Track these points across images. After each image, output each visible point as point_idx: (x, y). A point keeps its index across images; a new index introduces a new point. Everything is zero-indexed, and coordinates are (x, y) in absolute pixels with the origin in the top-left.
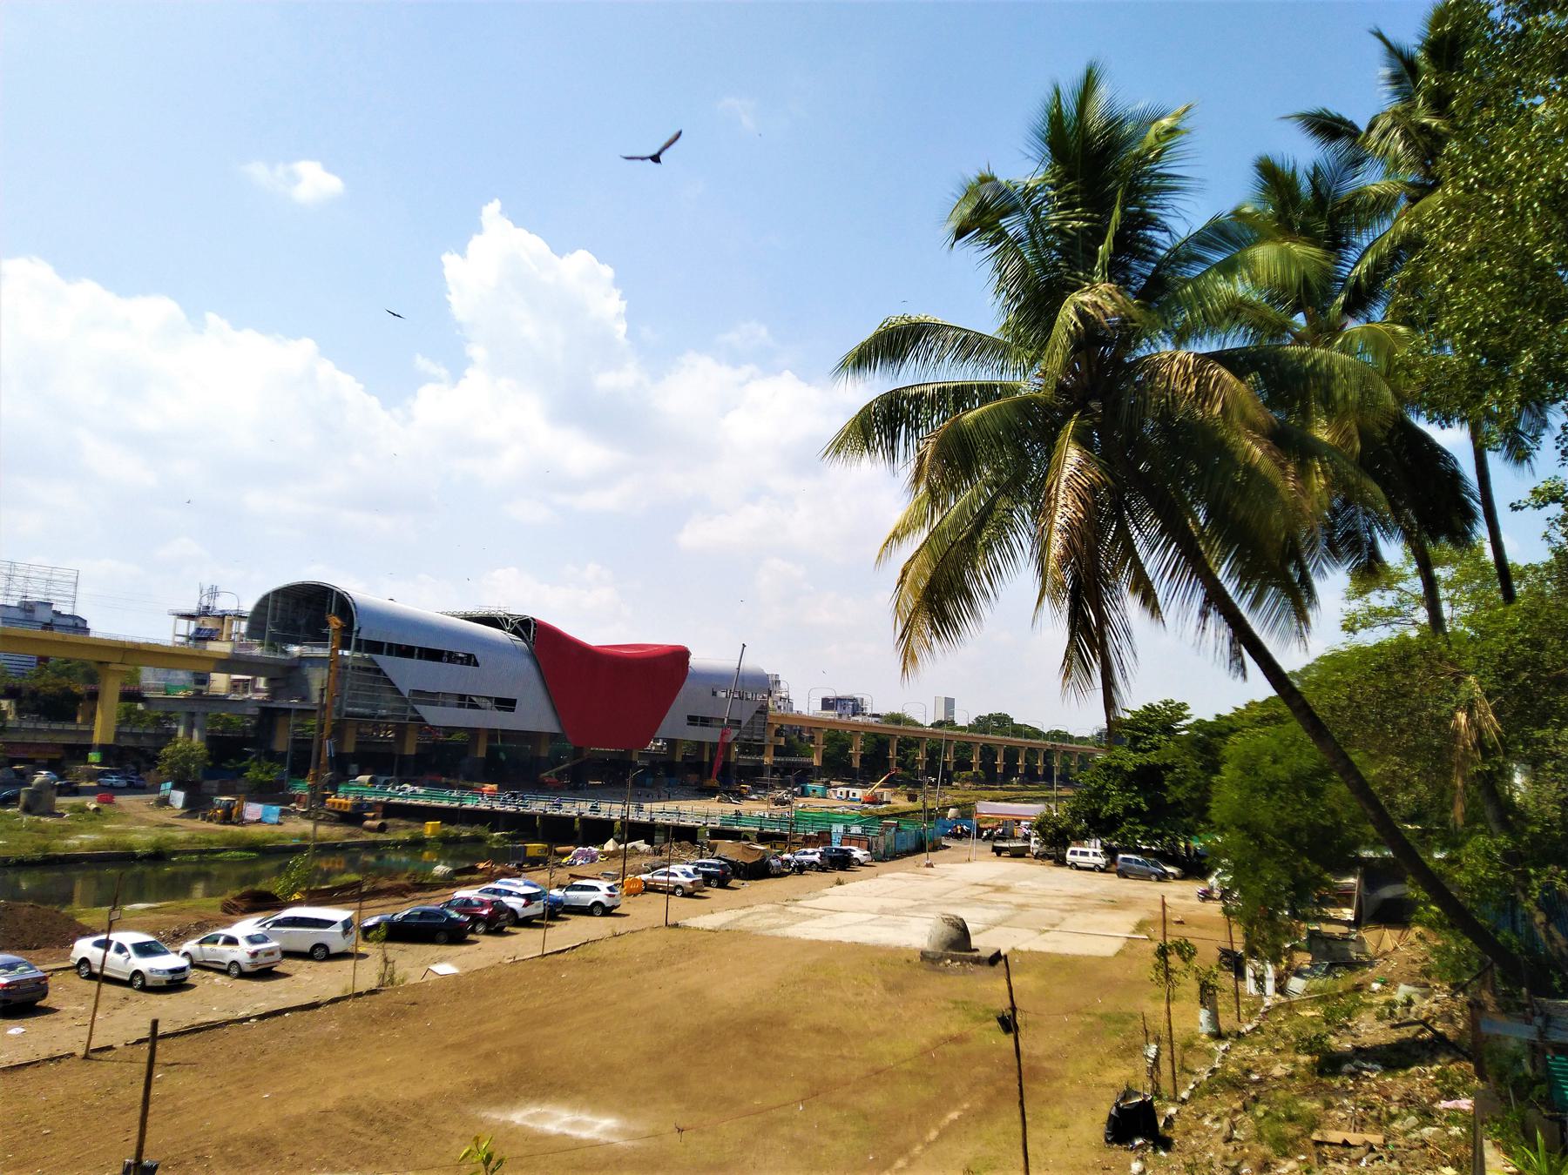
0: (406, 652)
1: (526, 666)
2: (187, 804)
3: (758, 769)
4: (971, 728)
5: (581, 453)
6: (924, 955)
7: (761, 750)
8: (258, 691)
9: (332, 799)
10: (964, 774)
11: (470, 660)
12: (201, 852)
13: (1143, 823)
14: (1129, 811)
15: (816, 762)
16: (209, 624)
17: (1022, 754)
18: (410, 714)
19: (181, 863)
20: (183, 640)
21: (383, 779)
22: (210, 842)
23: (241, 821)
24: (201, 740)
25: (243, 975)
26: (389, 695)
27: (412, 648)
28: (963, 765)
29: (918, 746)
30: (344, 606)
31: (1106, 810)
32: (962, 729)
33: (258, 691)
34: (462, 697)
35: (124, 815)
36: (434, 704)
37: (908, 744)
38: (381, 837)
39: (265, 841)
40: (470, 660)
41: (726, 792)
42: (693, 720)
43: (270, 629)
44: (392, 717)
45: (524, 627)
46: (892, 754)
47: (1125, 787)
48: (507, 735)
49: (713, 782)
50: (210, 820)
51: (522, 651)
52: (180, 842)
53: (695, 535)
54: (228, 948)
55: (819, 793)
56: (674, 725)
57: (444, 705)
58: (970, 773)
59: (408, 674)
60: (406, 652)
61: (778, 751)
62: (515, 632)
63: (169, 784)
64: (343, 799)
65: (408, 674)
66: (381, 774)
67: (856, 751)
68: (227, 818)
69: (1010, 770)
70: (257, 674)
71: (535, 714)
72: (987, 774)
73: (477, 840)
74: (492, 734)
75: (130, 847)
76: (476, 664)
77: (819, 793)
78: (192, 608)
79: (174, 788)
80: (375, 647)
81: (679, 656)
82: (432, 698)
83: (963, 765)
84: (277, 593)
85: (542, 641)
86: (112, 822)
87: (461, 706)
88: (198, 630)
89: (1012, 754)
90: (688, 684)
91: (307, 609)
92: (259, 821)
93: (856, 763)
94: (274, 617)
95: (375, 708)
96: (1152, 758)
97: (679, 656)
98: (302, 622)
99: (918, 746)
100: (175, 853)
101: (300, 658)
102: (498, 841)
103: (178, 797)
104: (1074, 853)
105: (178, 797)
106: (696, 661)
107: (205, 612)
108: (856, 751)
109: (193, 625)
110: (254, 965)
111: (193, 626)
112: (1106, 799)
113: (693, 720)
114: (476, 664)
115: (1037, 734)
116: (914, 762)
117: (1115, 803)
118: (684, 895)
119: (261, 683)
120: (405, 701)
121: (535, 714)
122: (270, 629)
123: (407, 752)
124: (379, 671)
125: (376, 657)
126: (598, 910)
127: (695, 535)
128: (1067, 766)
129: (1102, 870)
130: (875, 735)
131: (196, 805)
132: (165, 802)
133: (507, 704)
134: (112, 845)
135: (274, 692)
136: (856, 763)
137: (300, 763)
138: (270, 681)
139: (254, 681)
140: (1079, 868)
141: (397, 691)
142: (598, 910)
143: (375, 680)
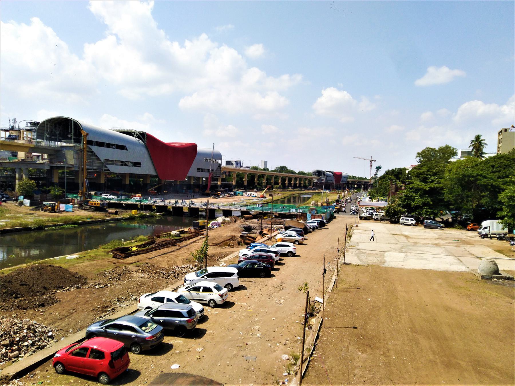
0: (100, 144)
1: (144, 150)
2: (31, 205)
3: (216, 186)
4: (275, 171)
5: (149, 71)
6: (483, 277)
7: (217, 180)
8: (43, 159)
9: (91, 202)
10: (276, 186)
11: (123, 148)
12: (56, 226)
13: (430, 208)
14: (424, 204)
15: (234, 183)
16: (14, 133)
17: (298, 180)
18: (104, 168)
19: (49, 230)
20: (3, 139)
21: (100, 192)
22: (57, 221)
23: (59, 212)
24: (26, 177)
25: (217, 306)
26: (96, 161)
27: (104, 143)
28: (276, 183)
29: (263, 177)
30: (77, 126)
31: (414, 204)
32: (272, 171)
33: (43, 159)
34: (122, 162)
35: (8, 210)
36: (113, 164)
37: (261, 176)
38: (116, 217)
39: (78, 220)
40: (123, 148)
41: (215, 195)
42: (198, 170)
43: (46, 135)
44: (98, 169)
45: (142, 136)
46: (256, 180)
47: (422, 196)
48: (140, 176)
49: (208, 191)
50: (46, 211)
51: (142, 145)
52: (44, 222)
53: (184, 103)
54: (206, 294)
55: (241, 194)
56: (193, 172)
57: (116, 165)
58: (278, 186)
59: (103, 153)
60: (100, 144)
61: (223, 180)
62: (138, 137)
63: (22, 197)
64: (96, 201)
65: (103, 153)
66: (99, 191)
67: (245, 179)
68: (53, 210)
69: (290, 184)
70: (43, 153)
71: (147, 168)
72: (283, 186)
73: (152, 216)
74: (132, 176)
75: (27, 225)
76: (127, 150)
77: (241, 194)
78: (7, 127)
79: (25, 198)
80: (90, 143)
81: (194, 147)
82: (112, 162)
83: (276, 183)
84: (47, 121)
85: (149, 141)
86: (10, 213)
87: (122, 165)
88: (10, 136)
89: (290, 179)
90: (197, 157)
91: (62, 128)
92: (64, 211)
93: (246, 183)
94: (47, 131)
95: (92, 166)
96: (432, 185)
97: (194, 147)
98: (58, 132)
99: (263, 177)
100: (46, 227)
101: (61, 147)
102: (159, 217)
103: (27, 202)
104: (403, 219)
105: (27, 202)
106: (199, 149)
107: (12, 129)
108: (245, 179)
109: (8, 134)
110: (222, 301)
111: (8, 134)
112: (414, 200)
113: (198, 170)
114: (127, 150)
115: (292, 172)
116: (262, 183)
117: (418, 201)
118: (299, 244)
119: (45, 156)
120: (102, 163)
121: (147, 168)
122: (46, 135)
123: (101, 182)
124: (92, 152)
125: (90, 146)
126: (290, 254)
127: (184, 103)
128: (305, 183)
129: (414, 225)
130: (250, 174)
131: (36, 205)
132: (22, 204)
133: (137, 165)
134: (21, 225)
135: (50, 160)
136: (246, 183)
137: (73, 188)
138: (49, 156)
139: (42, 156)
140: (405, 225)
141: (99, 160)
142: (290, 254)
143: (92, 155)
